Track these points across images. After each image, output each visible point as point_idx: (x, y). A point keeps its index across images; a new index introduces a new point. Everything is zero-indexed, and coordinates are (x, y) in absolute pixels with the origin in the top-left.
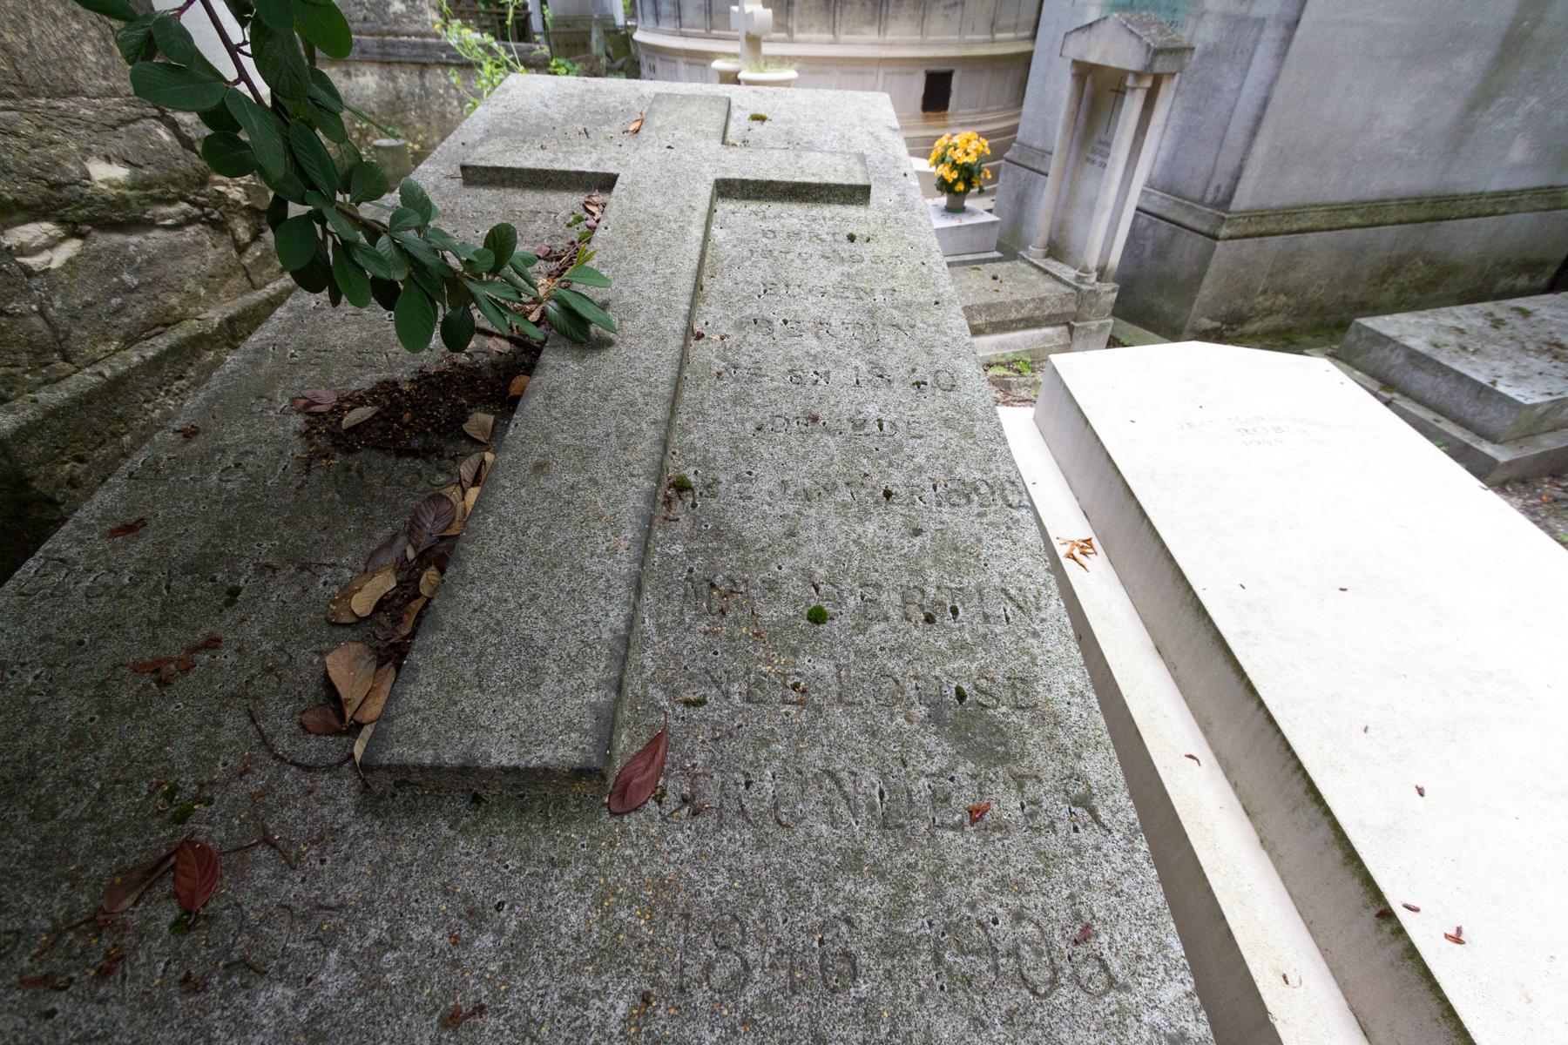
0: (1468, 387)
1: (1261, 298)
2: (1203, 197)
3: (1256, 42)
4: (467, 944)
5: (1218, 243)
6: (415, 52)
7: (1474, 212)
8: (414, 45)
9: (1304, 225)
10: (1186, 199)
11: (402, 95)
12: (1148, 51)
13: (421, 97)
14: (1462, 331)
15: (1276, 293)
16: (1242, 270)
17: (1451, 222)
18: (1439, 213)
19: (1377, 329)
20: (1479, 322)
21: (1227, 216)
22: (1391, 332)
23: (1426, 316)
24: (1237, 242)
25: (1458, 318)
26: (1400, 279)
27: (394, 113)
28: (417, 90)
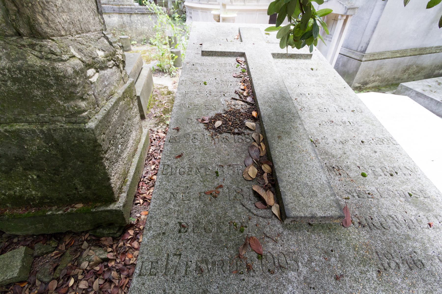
0: (434, 102)
1: (372, 78)
2: (357, 49)
3: (374, 6)
4: (329, 260)
5: (362, 63)
6: (129, 10)
7: (430, 52)
8: (128, 8)
9: (385, 57)
10: (352, 50)
11: (125, 23)
12: (346, 9)
13: (130, 23)
14: (430, 86)
15: (376, 76)
16: (368, 70)
17: (424, 55)
18: (421, 53)
19: (407, 86)
20: (434, 84)
21: (365, 55)
22: (411, 87)
23: (419, 82)
24: (367, 62)
25: (428, 82)
26: (409, 72)
27: (123, 28)
28: (129, 21)
